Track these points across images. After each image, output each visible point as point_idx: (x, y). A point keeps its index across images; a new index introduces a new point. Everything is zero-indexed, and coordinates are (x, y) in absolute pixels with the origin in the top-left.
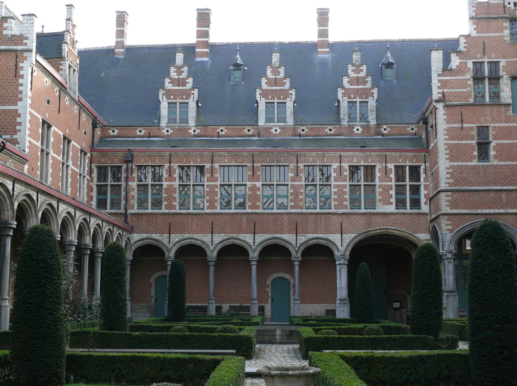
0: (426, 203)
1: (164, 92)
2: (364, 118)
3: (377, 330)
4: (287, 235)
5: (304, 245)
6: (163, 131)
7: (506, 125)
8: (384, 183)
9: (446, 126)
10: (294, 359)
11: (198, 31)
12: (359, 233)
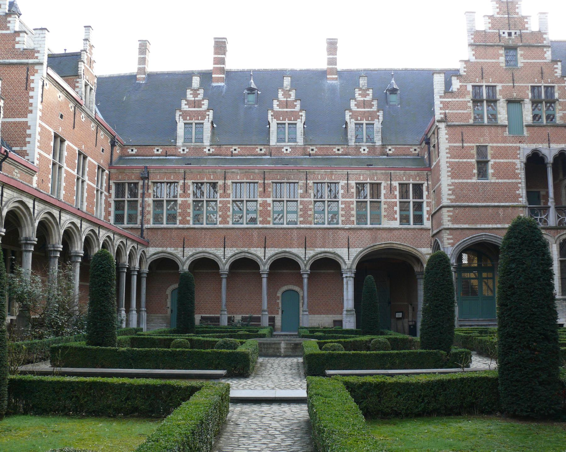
0: (428, 219)
1: (181, 113)
2: (370, 139)
3: (384, 343)
4: (296, 249)
5: (313, 259)
6: (179, 150)
7: (503, 145)
8: (389, 200)
9: (448, 145)
10: (295, 377)
11: (215, 58)
12: (365, 247)
